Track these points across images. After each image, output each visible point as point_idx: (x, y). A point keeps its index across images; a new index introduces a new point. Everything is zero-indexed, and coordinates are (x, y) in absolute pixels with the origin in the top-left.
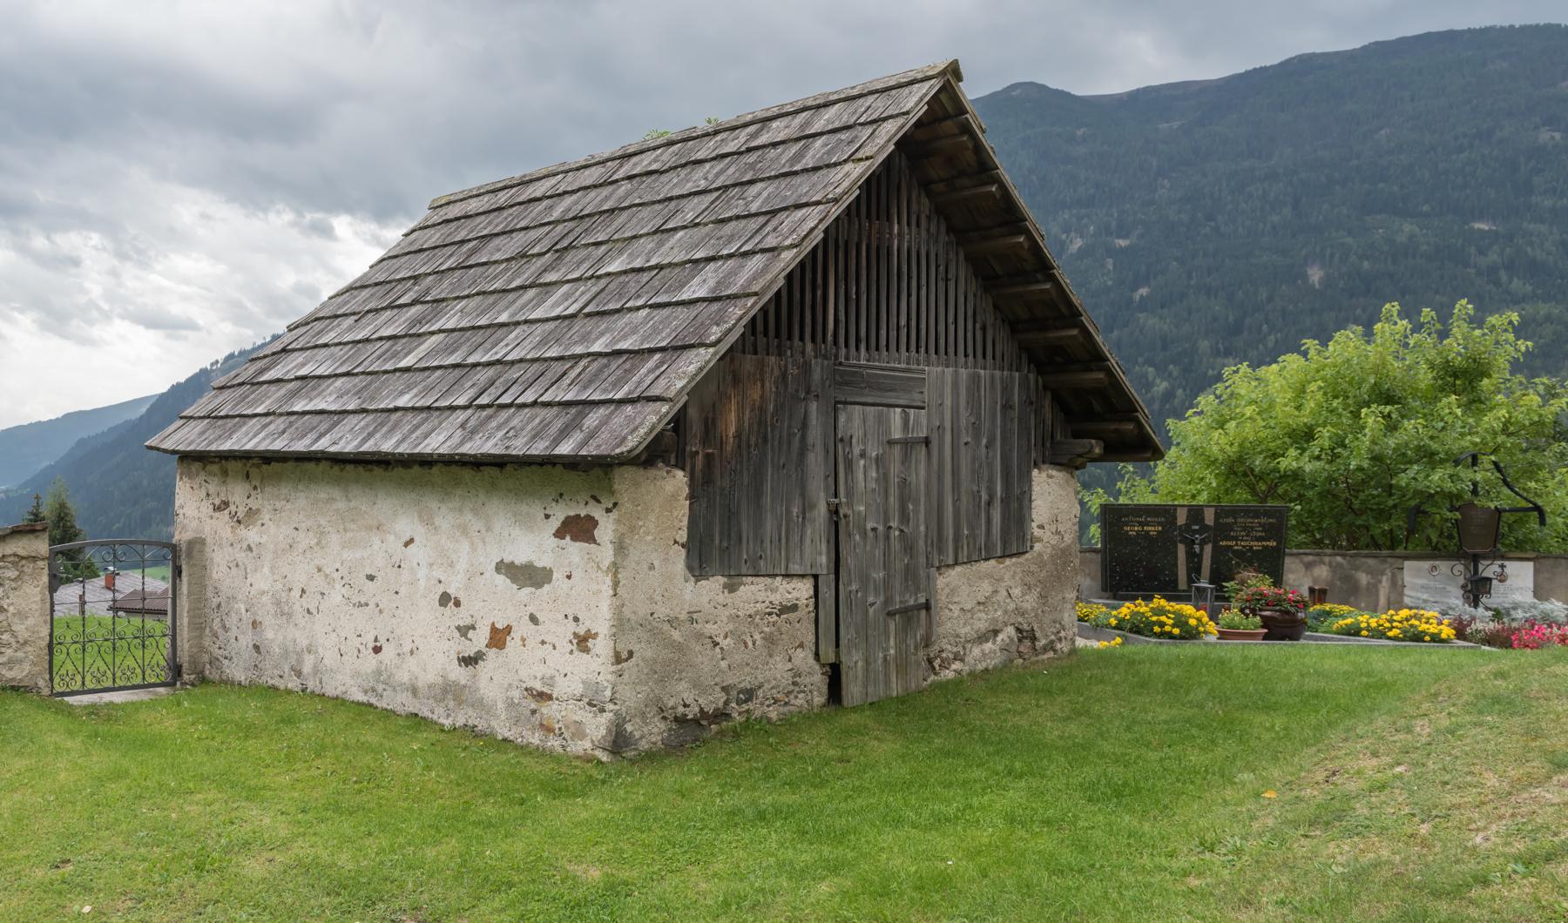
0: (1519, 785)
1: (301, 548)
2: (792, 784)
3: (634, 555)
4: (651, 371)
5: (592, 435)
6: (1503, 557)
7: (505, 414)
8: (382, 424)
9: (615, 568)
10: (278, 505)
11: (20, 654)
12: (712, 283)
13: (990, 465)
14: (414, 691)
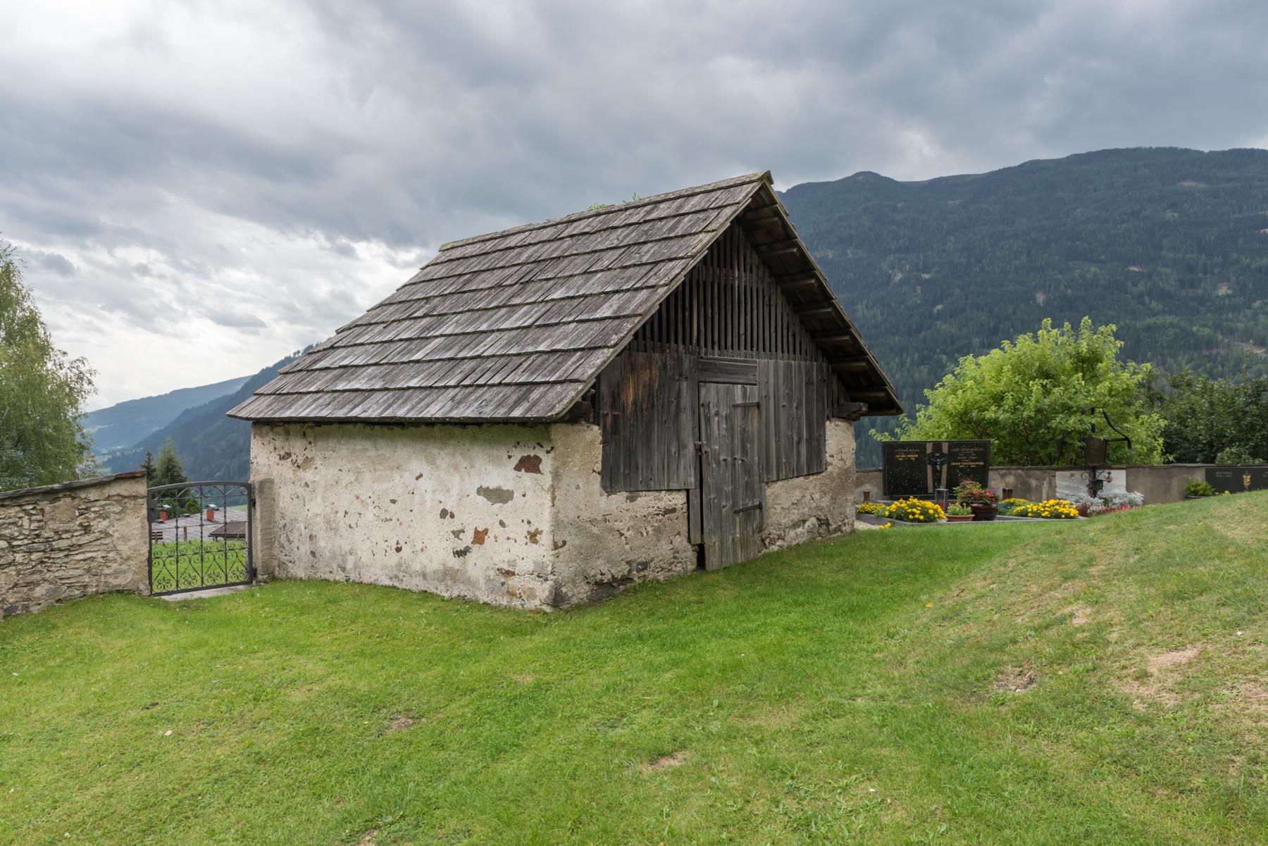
0: (1045, 590)
1: (344, 483)
2: (664, 618)
3: (565, 480)
4: (574, 363)
5: (534, 404)
6: (1110, 468)
7: (480, 391)
8: (398, 398)
9: (553, 489)
10: (327, 454)
11: (124, 567)
12: (615, 307)
13: (799, 419)
14: (424, 576)
